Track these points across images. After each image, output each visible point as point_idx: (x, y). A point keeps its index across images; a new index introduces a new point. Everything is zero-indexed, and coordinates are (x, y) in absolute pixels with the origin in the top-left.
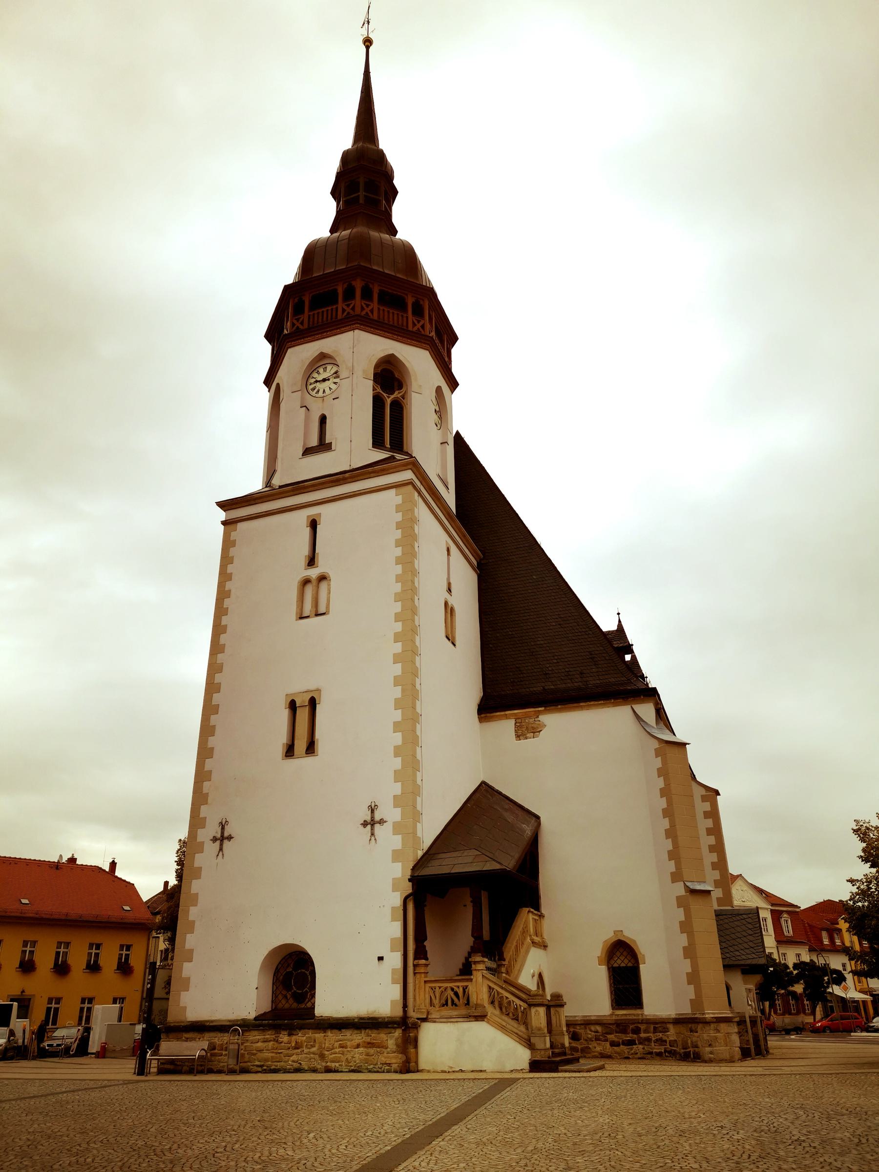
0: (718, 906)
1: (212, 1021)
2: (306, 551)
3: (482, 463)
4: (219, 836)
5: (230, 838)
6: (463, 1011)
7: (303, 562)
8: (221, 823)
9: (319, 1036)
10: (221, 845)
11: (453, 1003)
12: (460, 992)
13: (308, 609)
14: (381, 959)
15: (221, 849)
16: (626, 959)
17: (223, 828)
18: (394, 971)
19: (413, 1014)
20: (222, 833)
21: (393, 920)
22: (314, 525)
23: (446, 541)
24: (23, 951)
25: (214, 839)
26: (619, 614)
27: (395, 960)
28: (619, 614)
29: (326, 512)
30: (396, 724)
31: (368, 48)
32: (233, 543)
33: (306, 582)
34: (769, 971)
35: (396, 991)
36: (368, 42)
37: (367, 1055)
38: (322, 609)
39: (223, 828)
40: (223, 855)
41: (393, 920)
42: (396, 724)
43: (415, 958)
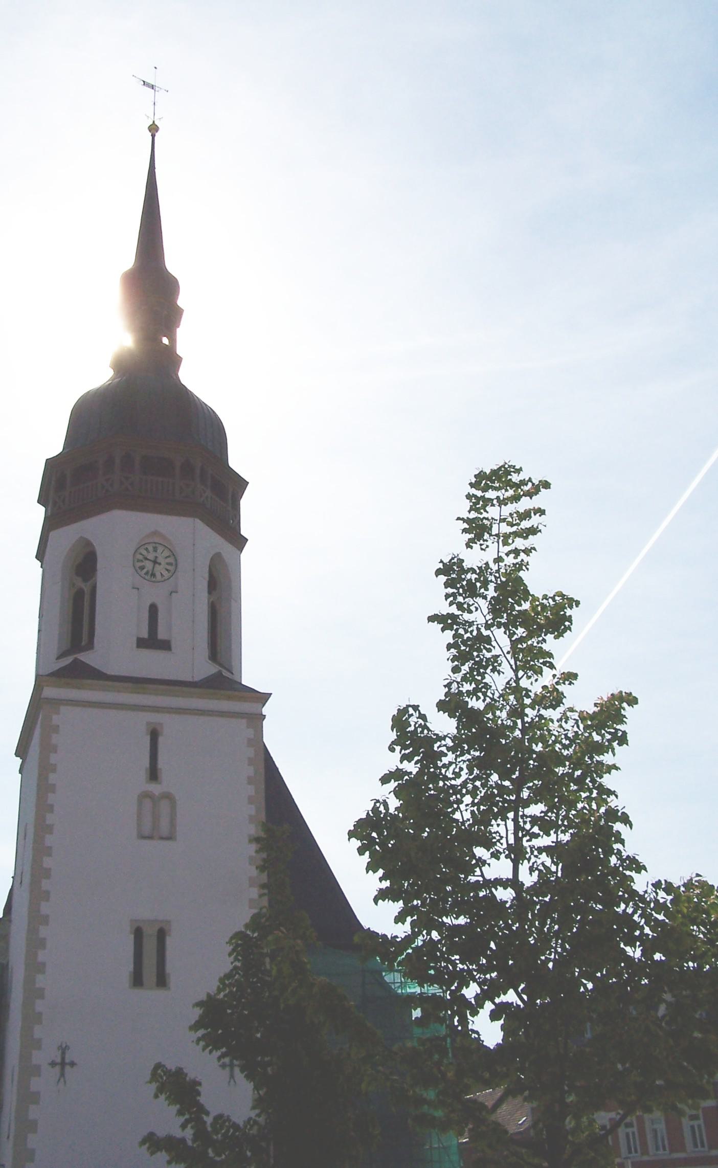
0: (361, 830)
3: (35, 655)
4: (59, 1060)
5: (72, 1064)
7: (143, 774)
8: (60, 1047)
10: (63, 1069)
13: (164, 806)
15: (62, 1075)
17: (63, 1053)
20: (63, 1058)
22: (154, 735)
23: (232, 673)
24: (146, 795)
25: (53, 1064)
29: (171, 725)
30: (250, 759)
31: (153, 136)
34: (403, 882)
36: (153, 129)
38: (164, 828)
39: (63, 1053)
40: (65, 1082)
42: (250, 759)
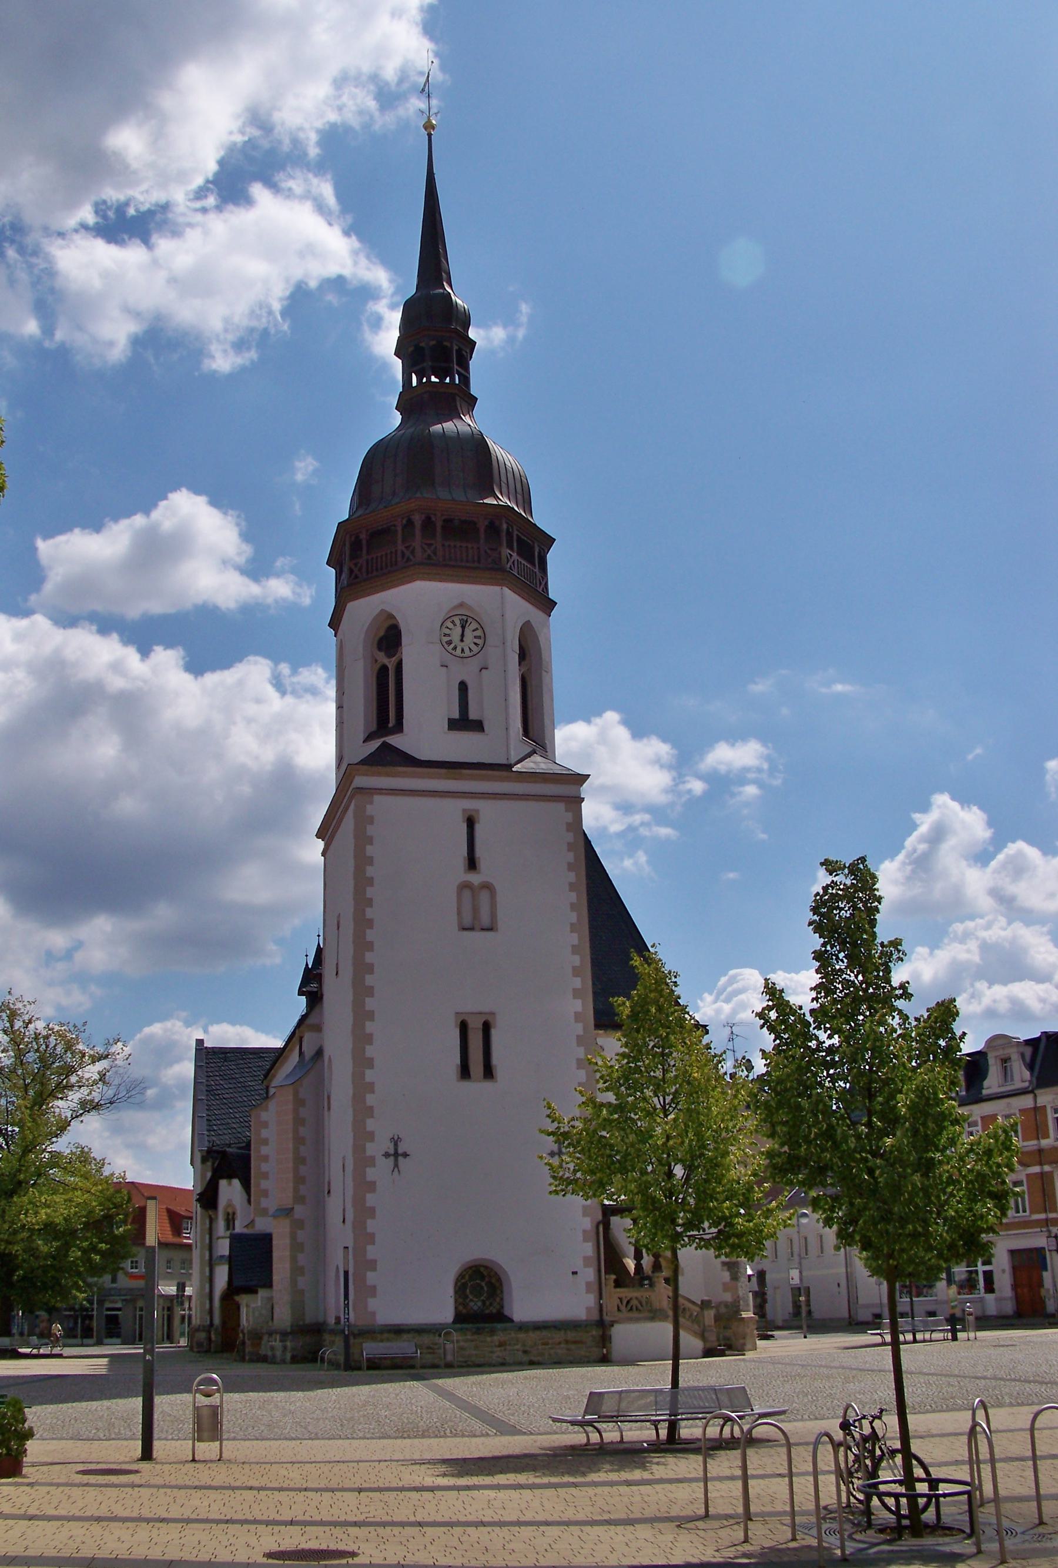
1: (407, 1325)
2: (479, 828)
5: (405, 1155)
6: (647, 1314)
9: (522, 1335)
11: (637, 1309)
12: (644, 1301)
14: (575, 1273)
16: (1029, 1490)
17: (396, 1145)
18: (588, 1284)
19: (607, 1318)
20: (396, 1150)
21: (585, 1240)
25: (387, 1155)
26: (307, 956)
27: (589, 1274)
28: (307, 956)
32: (369, 1039)
33: (465, 886)
35: (590, 1300)
37: (568, 1349)
38: (485, 920)
41: (585, 1240)
43: (606, 1273)
